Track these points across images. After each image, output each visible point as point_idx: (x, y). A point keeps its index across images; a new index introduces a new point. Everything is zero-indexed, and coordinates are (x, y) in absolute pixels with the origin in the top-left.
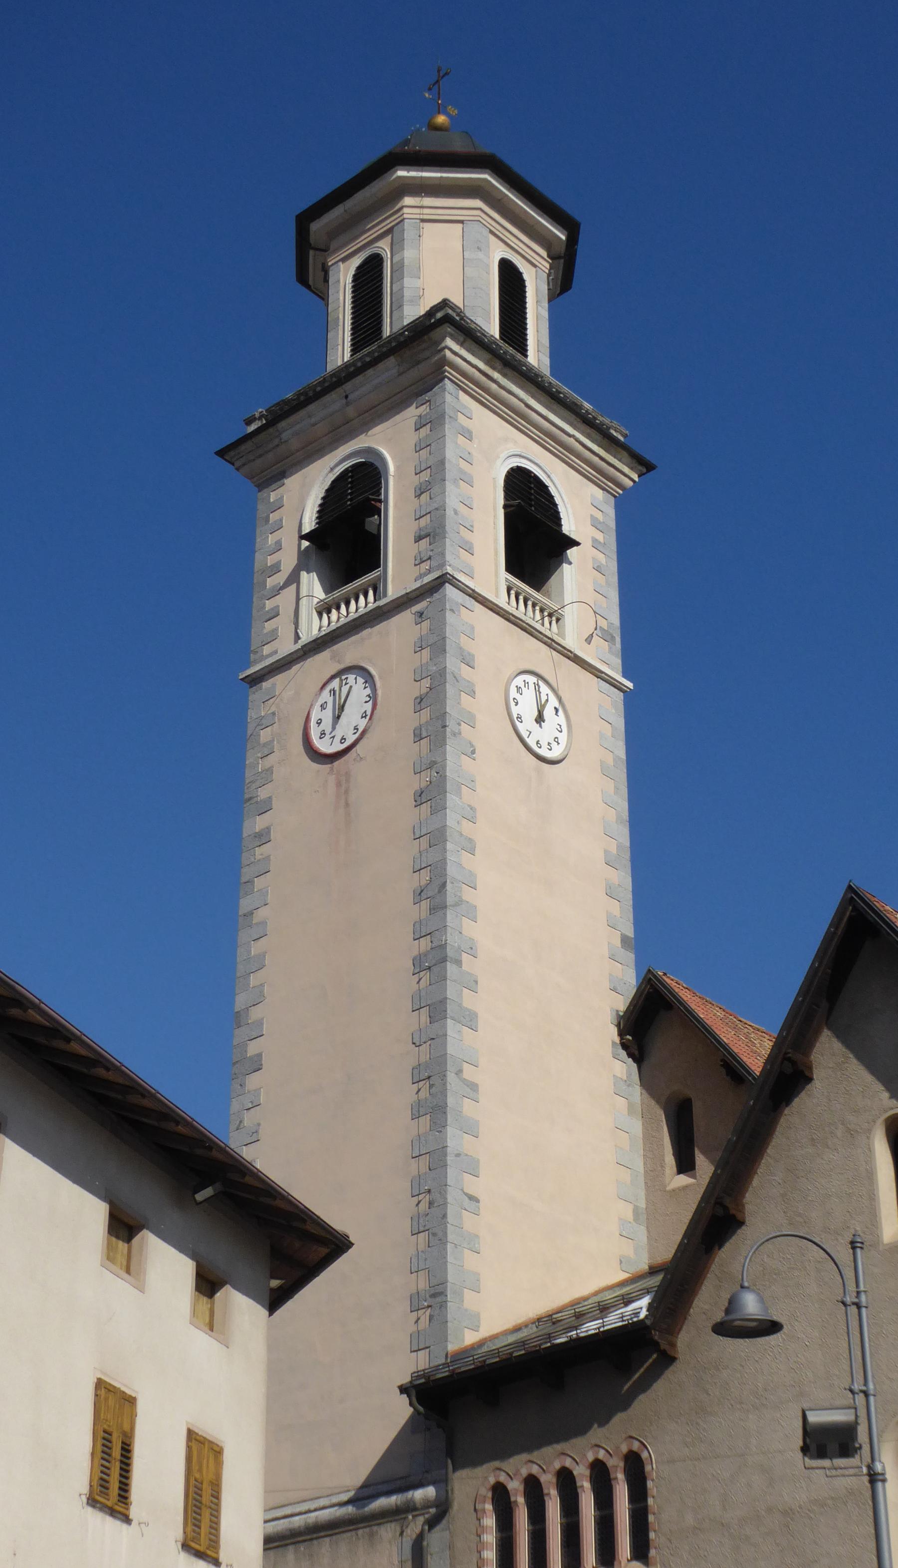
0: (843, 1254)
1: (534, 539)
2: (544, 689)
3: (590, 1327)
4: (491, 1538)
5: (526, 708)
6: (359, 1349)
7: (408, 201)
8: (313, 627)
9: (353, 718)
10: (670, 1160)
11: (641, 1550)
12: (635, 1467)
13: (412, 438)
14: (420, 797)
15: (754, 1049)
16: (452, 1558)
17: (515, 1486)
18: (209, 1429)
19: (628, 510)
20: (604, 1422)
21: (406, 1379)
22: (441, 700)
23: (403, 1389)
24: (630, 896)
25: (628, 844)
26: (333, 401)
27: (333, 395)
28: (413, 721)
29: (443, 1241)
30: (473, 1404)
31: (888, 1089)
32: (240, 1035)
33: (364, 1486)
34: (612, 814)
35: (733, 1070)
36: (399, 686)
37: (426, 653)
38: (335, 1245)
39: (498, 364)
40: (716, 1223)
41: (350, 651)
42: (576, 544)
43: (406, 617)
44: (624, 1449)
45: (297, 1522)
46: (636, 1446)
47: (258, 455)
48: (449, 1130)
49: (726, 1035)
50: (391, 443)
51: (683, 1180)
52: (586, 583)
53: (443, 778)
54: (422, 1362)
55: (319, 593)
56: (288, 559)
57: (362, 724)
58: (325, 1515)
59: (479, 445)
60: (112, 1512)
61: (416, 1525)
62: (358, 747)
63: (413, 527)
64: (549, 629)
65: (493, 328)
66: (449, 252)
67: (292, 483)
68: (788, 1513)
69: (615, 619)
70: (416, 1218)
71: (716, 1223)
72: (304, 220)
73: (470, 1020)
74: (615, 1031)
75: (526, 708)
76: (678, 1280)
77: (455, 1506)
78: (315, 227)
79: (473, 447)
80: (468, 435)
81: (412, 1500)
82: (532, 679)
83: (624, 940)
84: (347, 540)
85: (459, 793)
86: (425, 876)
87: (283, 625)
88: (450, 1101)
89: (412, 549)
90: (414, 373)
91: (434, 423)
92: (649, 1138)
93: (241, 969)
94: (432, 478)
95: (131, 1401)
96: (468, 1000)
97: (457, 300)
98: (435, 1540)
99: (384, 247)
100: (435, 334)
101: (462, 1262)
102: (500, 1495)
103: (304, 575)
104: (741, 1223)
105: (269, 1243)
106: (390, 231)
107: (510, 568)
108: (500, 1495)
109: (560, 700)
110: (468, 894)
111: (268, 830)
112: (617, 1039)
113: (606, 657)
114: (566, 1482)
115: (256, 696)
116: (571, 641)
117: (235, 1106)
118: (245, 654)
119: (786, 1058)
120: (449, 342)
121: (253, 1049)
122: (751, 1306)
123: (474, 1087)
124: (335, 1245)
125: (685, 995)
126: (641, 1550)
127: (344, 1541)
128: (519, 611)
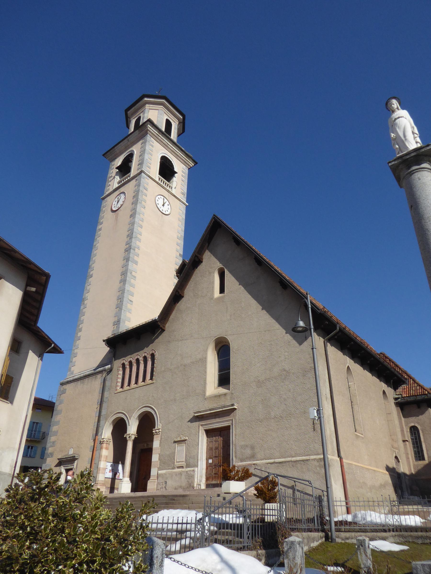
1: (167, 170)
2: (165, 200)
4: (120, 376)
5: (160, 202)
7: (147, 105)
9: (121, 202)
12: (153, 356)
16: (111, 381)
17: (127, 363)
21: (105, 338)
23: (104, 341)
24: (183, 246)
25: (183, 236)
27: (126, 140)
28: (132, 201)
31: (219, 261)
33: (98, 366)
34: (180, 229)
37: (137, 187)
39: (161, 133)
41: (122, 190)
42: (177, 173)
44: (151, 353)
45: (82, 375)
46: (153, 352)
47: (110, 154)
48: (126, 285)
56: (114, 174)
57: (122, 203)
58: (87, 373)
62: (121, 208)
63: (138, 163)
65: (163, 130)
68: (185, 366)
69: (186, 192)
70: (117, 305)
72: (127, 111)
73: (136, 263)
74: (175, 273)
75: (160, 202)
77: (114, 369)
78: (128, 112)
79: (153, 149)
81: (105, 368)
82: (163, 197)
83: (180, 255)
84: (124, 169)
85: (139, 215)
88: (128, 279)
100: (146, 124)
102: (123, 365)
103: (116, 177)
104: (183, 297)
106: (143, 111)
107: (159, 174)
108: (123, 365)
109: (164, 197)
111: (101, 228)
112: (176, 275)
115: (104, 201)
116: (174, 191)
117: (86, 285)
119: (196, 256)
120: (149, 126)
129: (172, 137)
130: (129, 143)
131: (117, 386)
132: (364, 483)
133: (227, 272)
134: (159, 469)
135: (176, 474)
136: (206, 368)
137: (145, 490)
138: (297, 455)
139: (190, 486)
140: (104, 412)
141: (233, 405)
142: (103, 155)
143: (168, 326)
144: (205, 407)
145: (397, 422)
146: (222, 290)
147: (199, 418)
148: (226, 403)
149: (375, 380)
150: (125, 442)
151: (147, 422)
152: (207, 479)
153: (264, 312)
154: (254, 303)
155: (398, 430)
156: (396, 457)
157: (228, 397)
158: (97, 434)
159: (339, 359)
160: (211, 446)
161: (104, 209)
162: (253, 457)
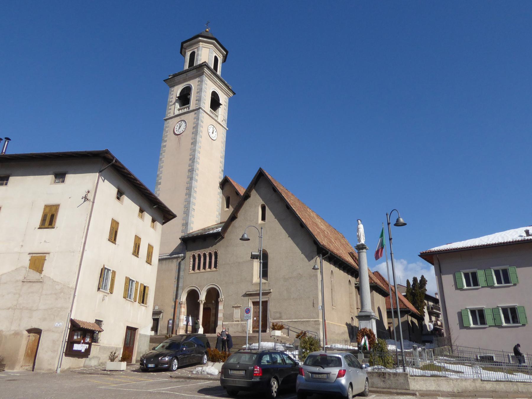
0: (260, 230)
1: (215, 103)
3: (211, 232)
4: (192, 263)
5: (211, 131)
6: (174, 231)
8: (177, 112)
10: (225, 206)
11: (215, 266)
12: (216, 254)
13: (197, 83)
14: (192, 143)
15: (242, 191)
17: (196, 256)
18: (152, 244)
19: (230, 100)
20: (212, 246)
22: (197, 128)
26: (184, 75)
28: (192, 131)
29: (188, 216)
30: (190, 242)
32: (158, 178)
35: (237, 193)
36: (190, 125)
38: (174, 216)
40: (233, 218)
41: (183, 117)
43: (193, 113)
47: (171, 82)
49: (237, 187)
50: (194, 84)
51: (227, 209)
52: (223, 111)
53: (196, 141)
54: (183, 234)
55: (178, 107)
56: (174, 100)
58: (165, 257)
59: (208, 86)
60: (136, 256)
61: (179, 260)
63: (196, 98)
64: (216, 118)
65: (212, 67)
66: (206, 53)
67: (176, 87)
68: (239, 263)
71: (233, 218)
73: (197, 181)
75: (211, 131)
76: (227, 225)
78: (184, 45)
80: (206, 84)
84: (184, 99)
86: (192, 157)
87: (172, 111)
89: (195, 102)
90: (199, 73)
91: (201, 82)
92: (222, 202)
93: (159, 168)
94: (200, 91)
95: (140, 239)
96: (196, 177)
97: (207, 62)
98: (182, 262)
99: (196, 50)
101: (191, 219)
105: (164, 214)
108: (194, 257)
110: (198, 160)
113: (225, 124)
114: (205, 255)
115: (166, 122)
116: (219, 121)
118: (164, 114)
121: (160, 181)
122: (246, 236)
123: (196, 191)
124: (174, 216)
125: (231, 180)
126: (215, 266)
127: (168, 261)
128: (212, 115)
129: (218, 73)
130: (187, 77)
131: (189, 269)
132: (334, 332)
133: (267, 208)
134: (223, 321)
135: (235, 325)
136: (253, 266)
137: (215, 333)
138: (304, 318)
139: (244, 331)
140: (180, 285)
141: (270, 290)
142: (164, 81)
143: (226, 235)
144: (252, 289)
145: (355, 298)
146: (263, 218)
147: (247, 295)
148: (266, 288)
149: (346, 274)
150: (198, 305)
151: (213, 295)
152: (253, 328)
153: (290, 239)
154: (284, 232)
155: (355, 302)
156: (352, 318)
157: (267, 285)
158: (176, 298)
159: (328, 267)
160: (255, 310)
161: (167, 129)
162: (280, 318)
